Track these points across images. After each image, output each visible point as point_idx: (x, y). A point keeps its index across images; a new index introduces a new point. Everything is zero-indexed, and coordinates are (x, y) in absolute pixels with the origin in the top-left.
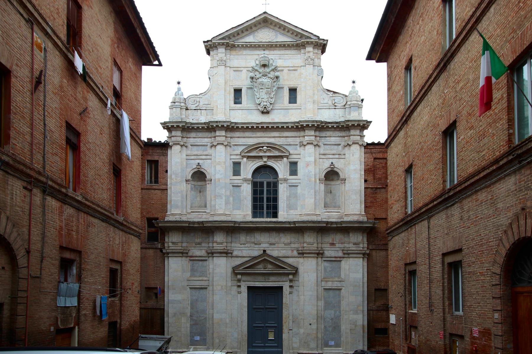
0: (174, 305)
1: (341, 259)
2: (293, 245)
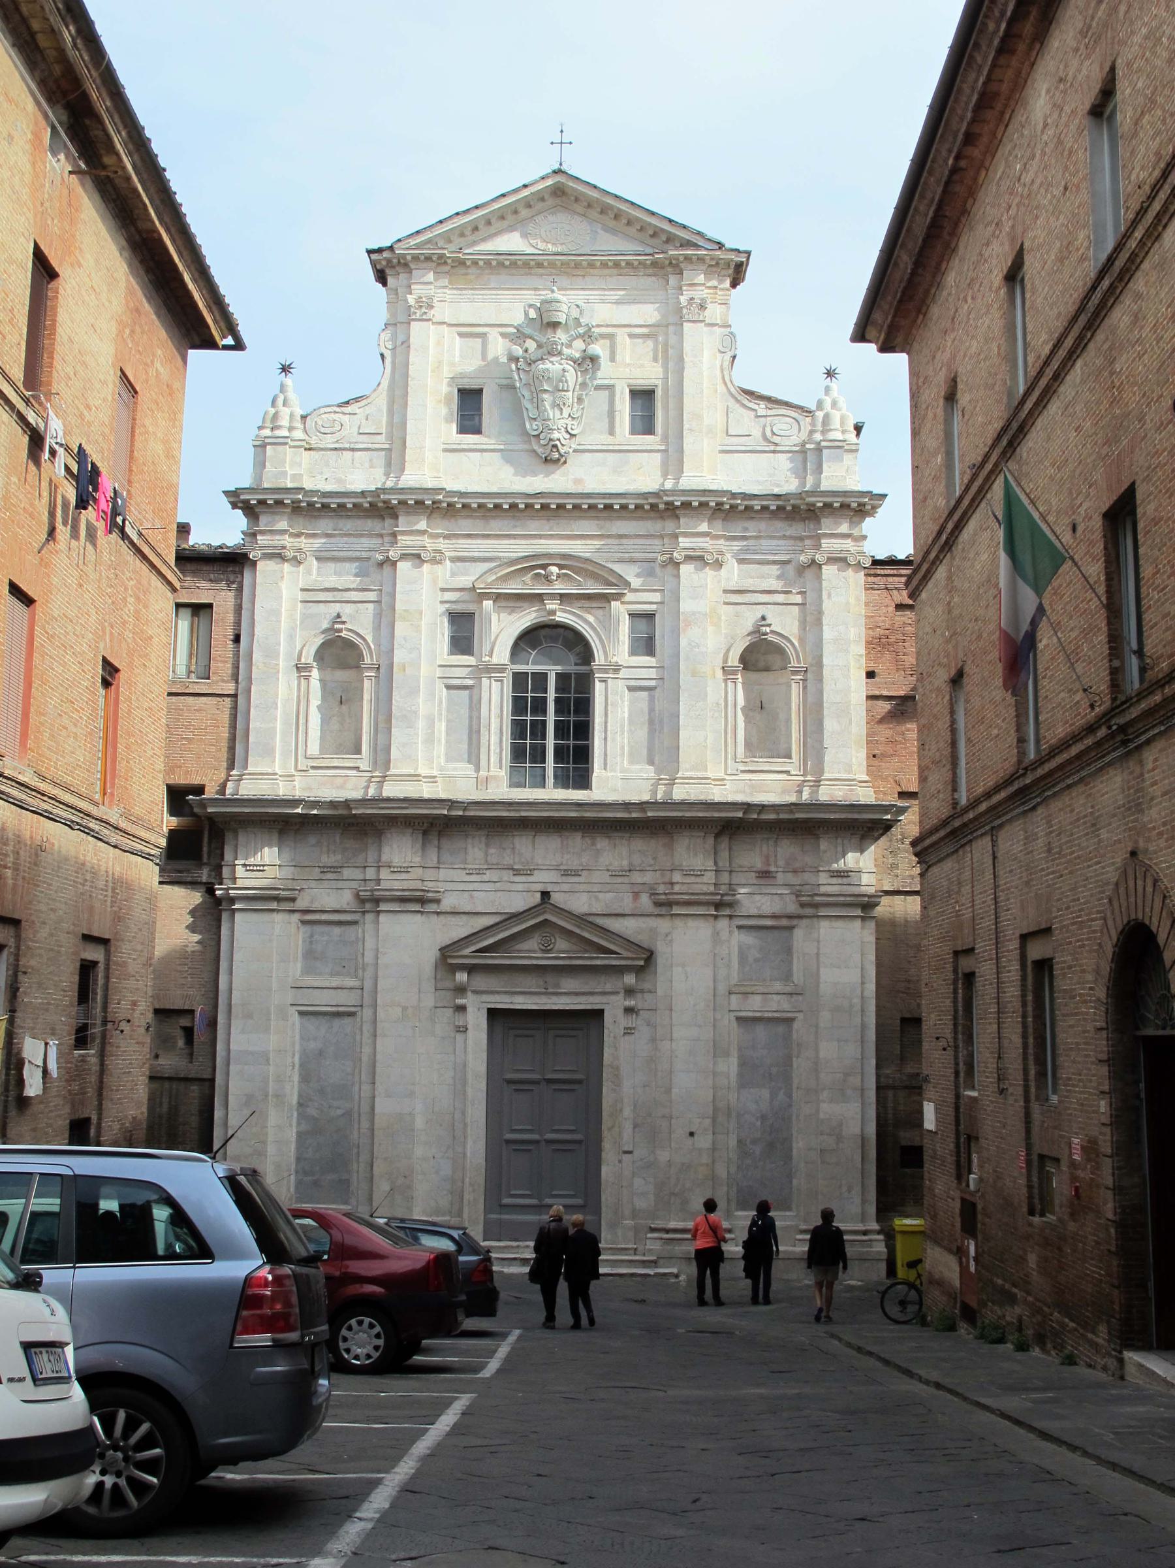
0: (246, 1067)
1: (795, 922)
2: (637, 878)
